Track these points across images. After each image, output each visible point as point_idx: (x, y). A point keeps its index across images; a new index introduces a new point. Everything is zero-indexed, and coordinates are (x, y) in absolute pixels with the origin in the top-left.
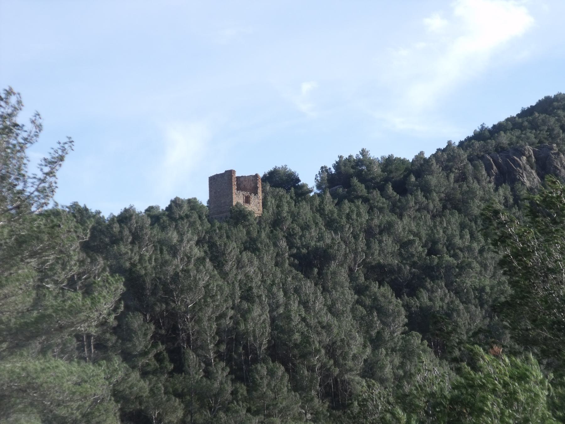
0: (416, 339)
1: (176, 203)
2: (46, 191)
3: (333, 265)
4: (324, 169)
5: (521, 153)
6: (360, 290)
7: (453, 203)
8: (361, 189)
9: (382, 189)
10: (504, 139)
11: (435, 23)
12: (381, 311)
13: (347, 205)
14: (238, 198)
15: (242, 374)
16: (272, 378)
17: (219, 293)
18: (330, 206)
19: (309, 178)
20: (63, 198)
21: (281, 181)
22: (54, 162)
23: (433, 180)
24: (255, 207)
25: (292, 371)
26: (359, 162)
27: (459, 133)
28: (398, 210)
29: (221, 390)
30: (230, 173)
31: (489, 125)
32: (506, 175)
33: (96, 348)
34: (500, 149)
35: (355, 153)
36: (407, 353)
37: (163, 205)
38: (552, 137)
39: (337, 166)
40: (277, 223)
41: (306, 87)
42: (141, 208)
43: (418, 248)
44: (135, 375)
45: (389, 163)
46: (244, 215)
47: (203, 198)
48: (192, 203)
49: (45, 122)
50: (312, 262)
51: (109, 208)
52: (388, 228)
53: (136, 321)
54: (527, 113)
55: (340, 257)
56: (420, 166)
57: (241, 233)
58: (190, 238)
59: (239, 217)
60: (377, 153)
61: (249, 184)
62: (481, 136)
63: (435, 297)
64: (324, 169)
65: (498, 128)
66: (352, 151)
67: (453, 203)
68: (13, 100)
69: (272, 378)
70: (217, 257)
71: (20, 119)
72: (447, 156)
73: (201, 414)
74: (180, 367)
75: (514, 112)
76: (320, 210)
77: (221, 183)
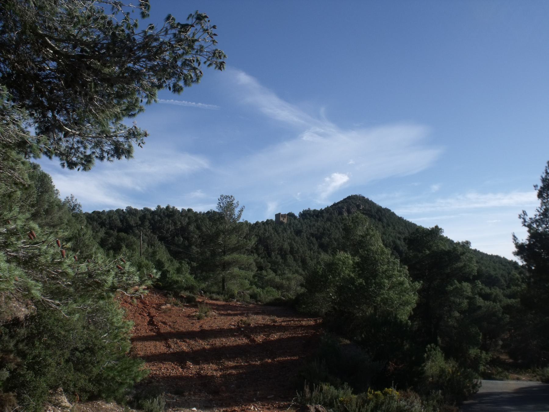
0: (320, 250)
1: (268, 220)
2: (239, 216)
3: (303, 234)
4: (300, 213)
5: (343, 208)
6: (308, 239)
7: (329, 220)
8: (308, 216)
9: (313, 216)
10: (340, 205)
11: (327, 179)
12: (313, 244)
13: (305, 220)
14: (281, 219)
15: (284, 257)
16: (290, 259)
17: (25, 341)
18: (302, 220)
19: (297, 214)
20: (241, 220)
21: (291, 215)
22: (241, 211)
23: (324, 215)
24: (285, 221)
25: (294, 257)
26: (308, 211)
27: (330, 204)
28: (317, 221)
29: (279, 262)
30: (280, 214)
31: (336, 202)
32: (340, 213)
33: (251, 252)
34: (339, 207)
35: (307, 209)
36: (319, 253)
37: (265, 221)
38: (350, 205)
39: (303, 212)
40: (290, 224)
41: (299, 194)
42: (260, 221)
43: (321, 230)
44: (260, 258)
45: (315, 211)
46: (282, 223)
47: (274, 219)
48: (271, 220)
49: (239, 203)
50: (298, 233)
51: (252, 221)
52: (314, 225)
53: (260, 246)
54: (345, 199)
55: (304, 231)
56: (322, 211)
57: (282, 227)
58: (271, 229)
59: (282, 223)
60: (312, 209)
61: (284, 216)
62: (335, 205)
63: (325, 240)
64: (300, 213)
65: (338, 203)
66: (306, 208)
67: (329, 220)
68: (232, 198)
69: (290, 259)
70: (276, 231)
71: (234, 202)
72: (327, 209)
73: (541, 227)
74: (270, 256)
75: (342, 199)
76: (299, 221)
77: (278, 216)
